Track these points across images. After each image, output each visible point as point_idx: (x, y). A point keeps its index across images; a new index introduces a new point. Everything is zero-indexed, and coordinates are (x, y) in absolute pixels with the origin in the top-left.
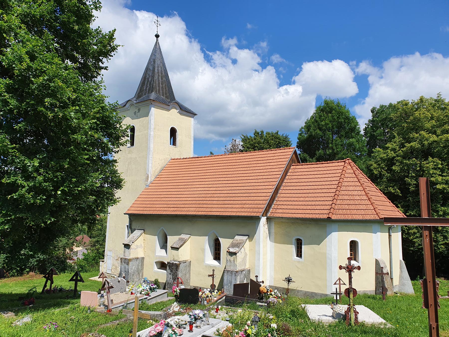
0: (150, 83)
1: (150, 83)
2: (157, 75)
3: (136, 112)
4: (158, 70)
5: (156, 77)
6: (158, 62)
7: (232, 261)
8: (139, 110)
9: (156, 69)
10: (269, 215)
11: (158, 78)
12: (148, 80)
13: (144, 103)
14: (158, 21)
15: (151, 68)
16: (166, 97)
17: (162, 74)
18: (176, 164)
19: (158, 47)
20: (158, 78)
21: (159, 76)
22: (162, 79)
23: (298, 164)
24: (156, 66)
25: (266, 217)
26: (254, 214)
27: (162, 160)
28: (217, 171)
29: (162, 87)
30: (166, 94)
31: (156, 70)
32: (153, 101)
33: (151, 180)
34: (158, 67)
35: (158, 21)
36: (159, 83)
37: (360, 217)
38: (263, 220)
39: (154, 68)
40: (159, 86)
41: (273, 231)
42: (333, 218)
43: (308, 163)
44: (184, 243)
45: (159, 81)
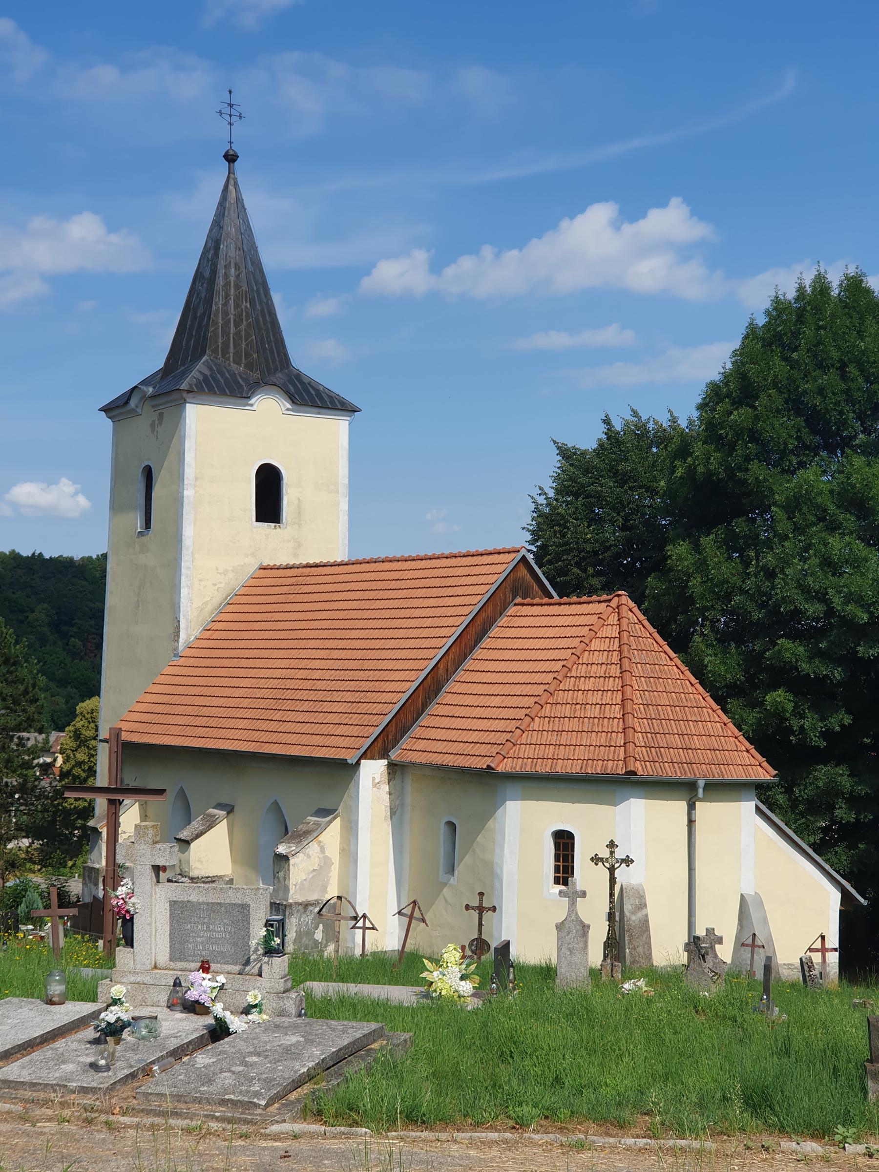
0: (200, 323)
1: (200, 323)
2: (222, 293)
3: (154, 421)
4: (226, 276)
5: (218, 303)
6: (229, 250)
7: (281, 879)
8: (161, 415)
9: (221, 272)
10: (394, 754)
11: (226, 304)
12: (195, 313)
13: (166, 399)
14: (231, 105)
15: (207, 274)
16: (249, 366)
17: (237, 287)
18: (279, 588)
19: (232, 194)
20: (226, 304)
21: (227, 296)
22: (237, 306)
23: (546, 600)
24: (221, 263)
25: (385, 762)
26: (341, 755)
27: (225, 572)
28: (341, 615)
29: (238, 334)
30: (248, 355)
31: (220, 281)
32: (189, 392)
33: (189, 636)
34: (227, 267)
35: (231, 105)
36: (227, 323)
37: (574, 768)
38: (373, 771)
39: (214, 272)
40: (226, 333)
41: (409, 799)
42: (500, 769)
43: (537, 600)
44: (210, 827)
45: (226, 313)
